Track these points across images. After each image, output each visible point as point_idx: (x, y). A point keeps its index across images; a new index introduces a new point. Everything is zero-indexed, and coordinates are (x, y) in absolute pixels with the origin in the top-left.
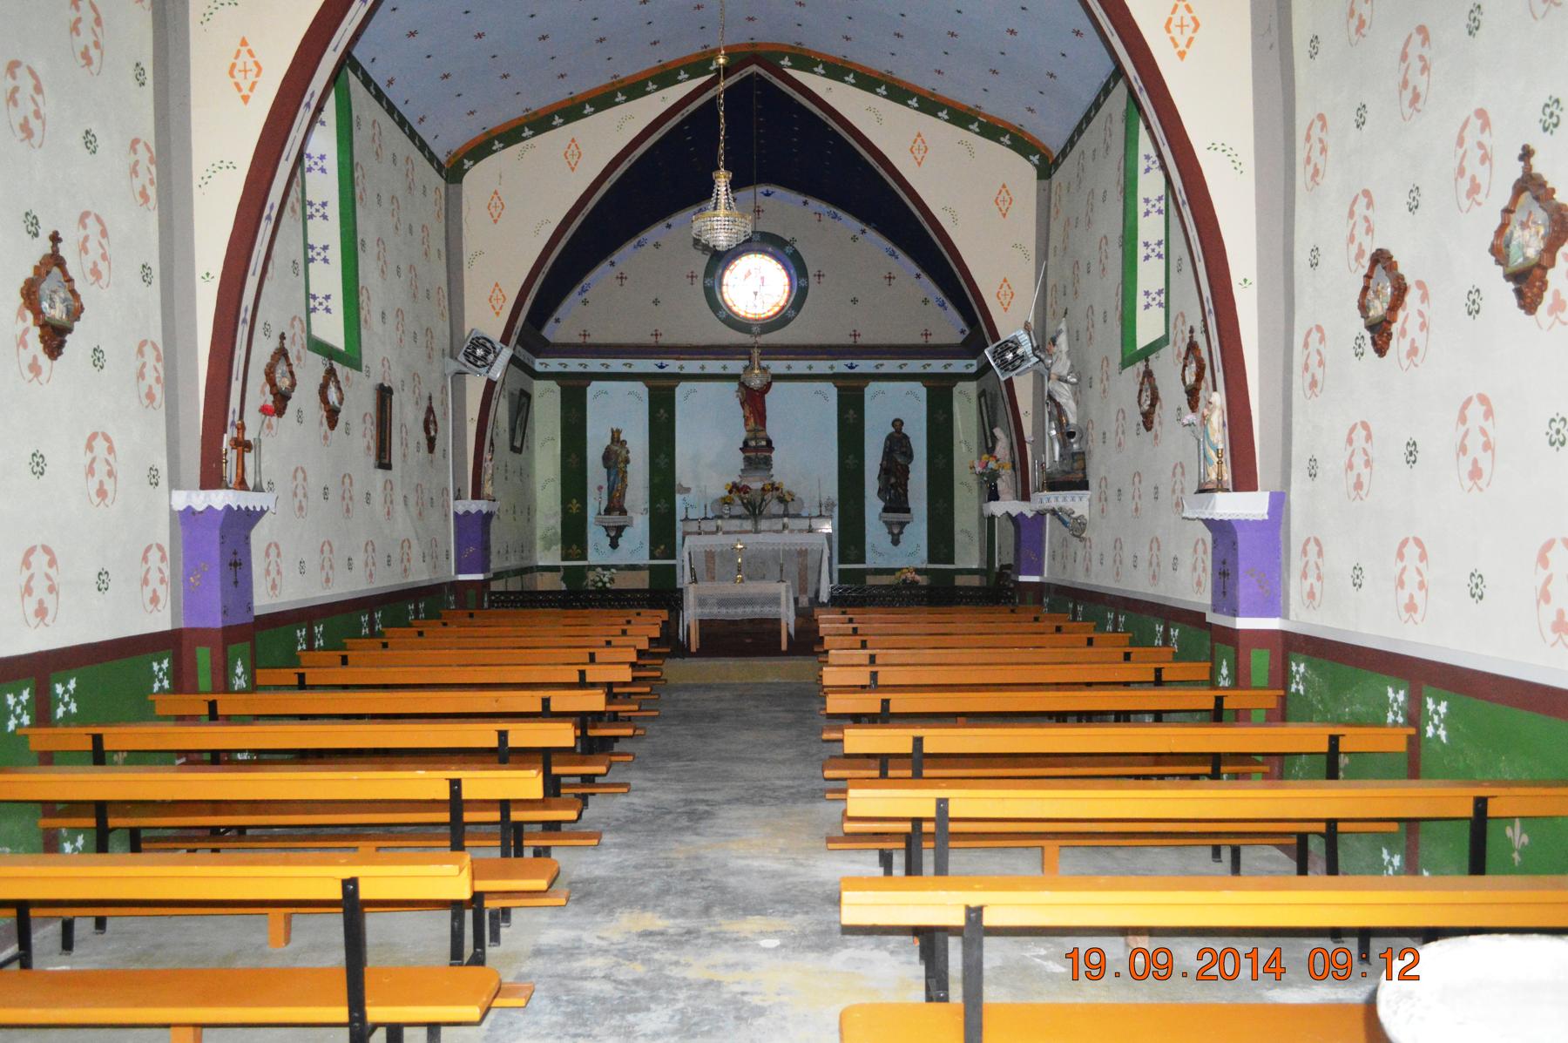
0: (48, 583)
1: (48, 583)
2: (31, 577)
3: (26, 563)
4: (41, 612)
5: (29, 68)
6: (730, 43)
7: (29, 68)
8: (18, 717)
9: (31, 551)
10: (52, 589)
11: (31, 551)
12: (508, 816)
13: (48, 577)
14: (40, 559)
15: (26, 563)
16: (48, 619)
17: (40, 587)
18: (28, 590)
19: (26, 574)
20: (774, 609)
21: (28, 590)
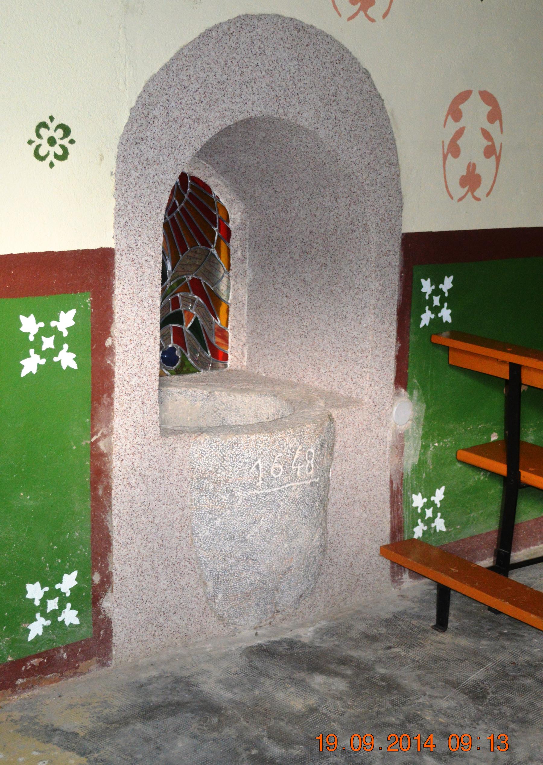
0: (486, 143)
1: (486, 143)
2: (460, 133)
3: (455, 113)
4: (471, 180)
5: (452, 198)
6: (117, 256)
7: (452, 198)
8: (436, 310)
9: (464, 96)
10: (490, 151)
11: (464, 96)
12: (430, 499)
13: (486, 135)
14: (475, 112)
15: (455, 113)
16: (480, 192)
17: (472, 147)
18: (454, 149)
19: (453, 127)
20: (189, 201)
21: (454, 149)
